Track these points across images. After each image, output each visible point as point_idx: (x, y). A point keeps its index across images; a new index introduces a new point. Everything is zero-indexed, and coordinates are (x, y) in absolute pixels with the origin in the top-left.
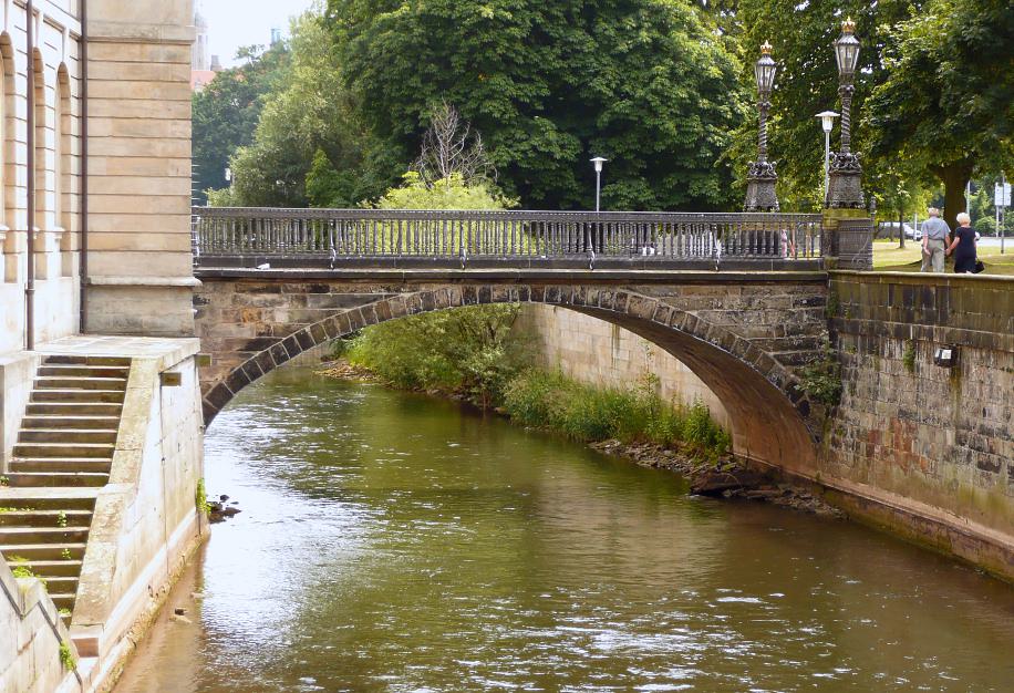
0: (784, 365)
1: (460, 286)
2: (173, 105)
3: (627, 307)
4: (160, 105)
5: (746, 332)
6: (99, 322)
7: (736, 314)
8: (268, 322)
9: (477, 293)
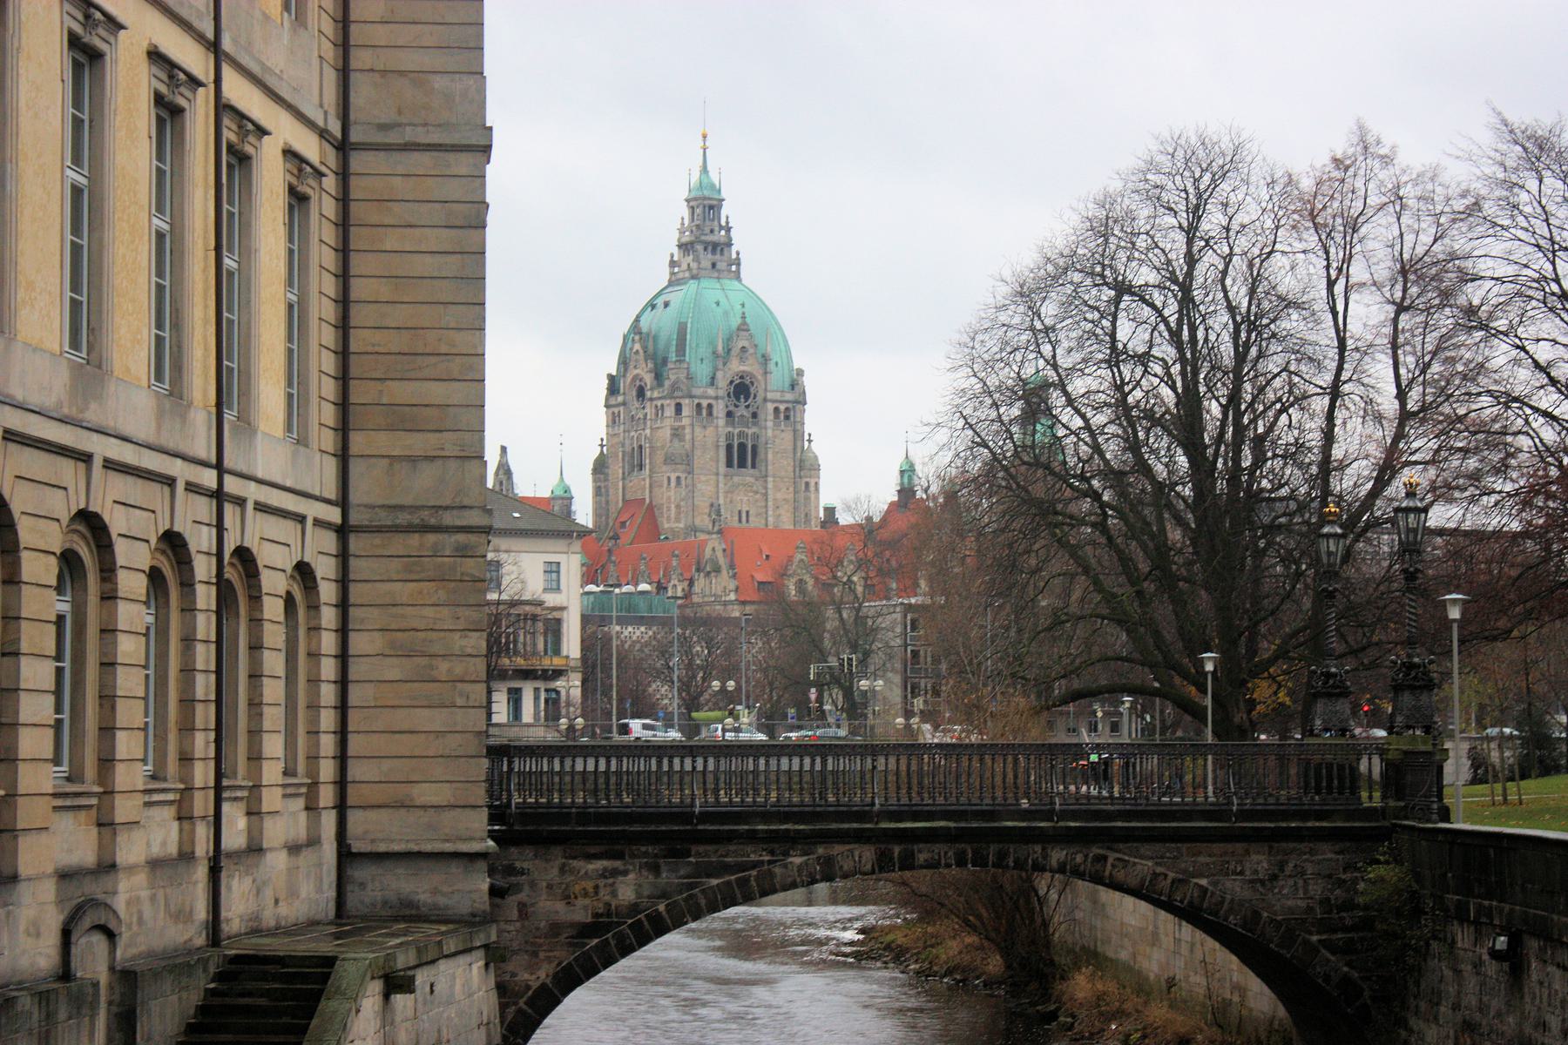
0: (1333, 953)
1: (873, 849)
3: (1107, 873)
4: (445, 611)
5: (1277, 908)
6: (362, 902)
7: (1262, 882)
8: (607, 898)
9: (896, 854)
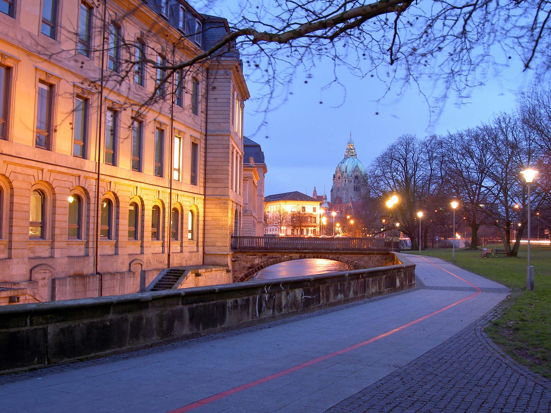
2: (224, 214)
